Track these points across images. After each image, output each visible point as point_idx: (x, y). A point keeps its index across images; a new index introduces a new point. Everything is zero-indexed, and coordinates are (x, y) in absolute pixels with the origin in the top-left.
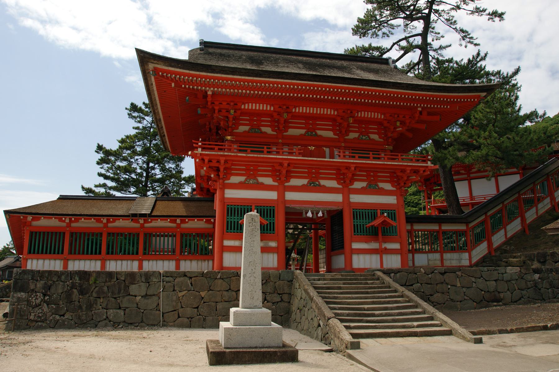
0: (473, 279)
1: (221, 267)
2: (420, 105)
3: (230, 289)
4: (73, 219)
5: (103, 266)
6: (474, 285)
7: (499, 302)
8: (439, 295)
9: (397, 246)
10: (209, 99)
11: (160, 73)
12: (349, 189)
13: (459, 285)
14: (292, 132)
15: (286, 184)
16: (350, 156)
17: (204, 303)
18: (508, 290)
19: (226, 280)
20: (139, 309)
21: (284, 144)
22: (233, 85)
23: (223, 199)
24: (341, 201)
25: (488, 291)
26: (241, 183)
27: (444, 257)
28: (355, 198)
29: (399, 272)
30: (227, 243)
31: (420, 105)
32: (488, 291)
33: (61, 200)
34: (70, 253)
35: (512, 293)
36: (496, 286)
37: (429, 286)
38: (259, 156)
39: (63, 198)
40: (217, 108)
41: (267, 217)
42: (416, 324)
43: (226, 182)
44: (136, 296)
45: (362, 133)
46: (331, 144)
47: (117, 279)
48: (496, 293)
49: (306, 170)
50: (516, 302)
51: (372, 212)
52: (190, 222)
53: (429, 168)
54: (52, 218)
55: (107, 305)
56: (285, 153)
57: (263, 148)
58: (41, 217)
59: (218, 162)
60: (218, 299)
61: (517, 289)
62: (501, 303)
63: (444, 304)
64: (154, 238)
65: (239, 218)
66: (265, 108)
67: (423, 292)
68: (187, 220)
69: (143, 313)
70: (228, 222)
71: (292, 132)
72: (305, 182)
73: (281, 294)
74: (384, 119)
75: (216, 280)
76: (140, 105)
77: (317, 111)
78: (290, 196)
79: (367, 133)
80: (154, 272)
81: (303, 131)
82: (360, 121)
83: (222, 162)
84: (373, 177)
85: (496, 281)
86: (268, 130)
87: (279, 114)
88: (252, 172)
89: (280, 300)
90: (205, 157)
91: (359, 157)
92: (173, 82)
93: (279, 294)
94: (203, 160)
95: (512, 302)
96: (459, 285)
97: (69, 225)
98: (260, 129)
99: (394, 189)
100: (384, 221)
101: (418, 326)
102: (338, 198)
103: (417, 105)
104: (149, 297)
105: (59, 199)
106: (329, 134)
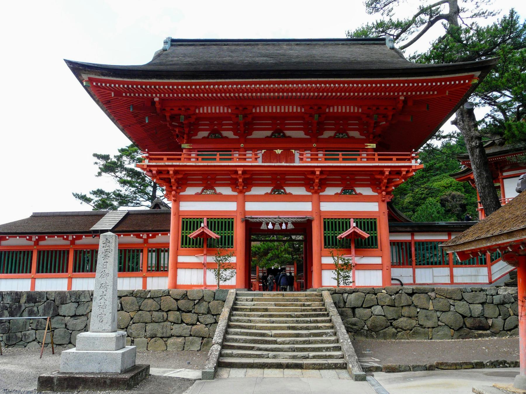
0: (451, 302)
1: (175, 286)
2: (403, 94)
3: (160, 309)
4: (150, 235)
5: (70, 285)
6: (452, 308)
7: (487, 330)
8: (405, 319)
9: (378, 260)
10: (158, 106)
11: (94, 84)
12: (320, 196)
13: (431, 308)
14: (257, 134)
15: (247, 193)
16: (368, 159)
17: (134, 323)
18: (500, 315)
19: (139, 298)
20: (68, 329)
21: (246, 149)
22: (317, 87)
23: (178, 212)
24: (311, 210)
25: (471, 316)
26: (197, 194)
27: (455, 274)
28: (326, 207)
29: (354, 292)
30: (181, 259)
31: (403, 94)
32: (471, 316)
33: (36, 219)
34: (38, 272)
35: (505, 320)
36: (483, 310)
37: (392, 308)
38: (209, 164)
39: (36, 216)
40: (168, 114)
41: (218, 230)
42: (312, 354)
43: (181, 194)
44: (64, 316)
45: (339, 131)
46: (302, 145)
47: (47, 299)
48: (483, 319)
49: (270, 177)
50: (510, 330)
51: (334, 224)
52: (11, 239)
53: (414, 168)
54: (16, 237)
55: (37, 325)
56: (363, 160)
57: (374, 155)
58: (82, 236)
59: (168, 172)
60: (148, 320)
61: (512, 314)
62: (488, 332)
63: (411, 330)
64: (162, 254)
65: (188, 231)
66: (222, 111)
67: (384, 316)
68: (7, 238)
69: (71, 333)
70: (183, 236)
71: (257, 134)
72: (268, 190)
73: (216, 315)
74: (231, 114)
75: (146, 301)
76: (113, 153)
77: (334, 109)
78: (251, 206)
79: (344, 131)
80: (84, 291)
81: (269, 133)
82: (337, 117)
83: (171, 172)
84: (349, 182)
85: (483, 304)
86: (230, 134)
87: (312, 116)
88: (209, 180)
89: (213, 321)
90: (152, 169)
91: (397, 159)
92: (112, 91)
93: (213, 315)
94: (151, 171)
95: (504, 330)
96: (431, 308)
97: (73, 242)
98: (221, 134)
99: (376, 194)
100: (354, 231)
101: (314, 357)
102: (306, 207)
103: (398, 94)
104: (79, 317)
105: (32, 216)
106: (300, 134)
